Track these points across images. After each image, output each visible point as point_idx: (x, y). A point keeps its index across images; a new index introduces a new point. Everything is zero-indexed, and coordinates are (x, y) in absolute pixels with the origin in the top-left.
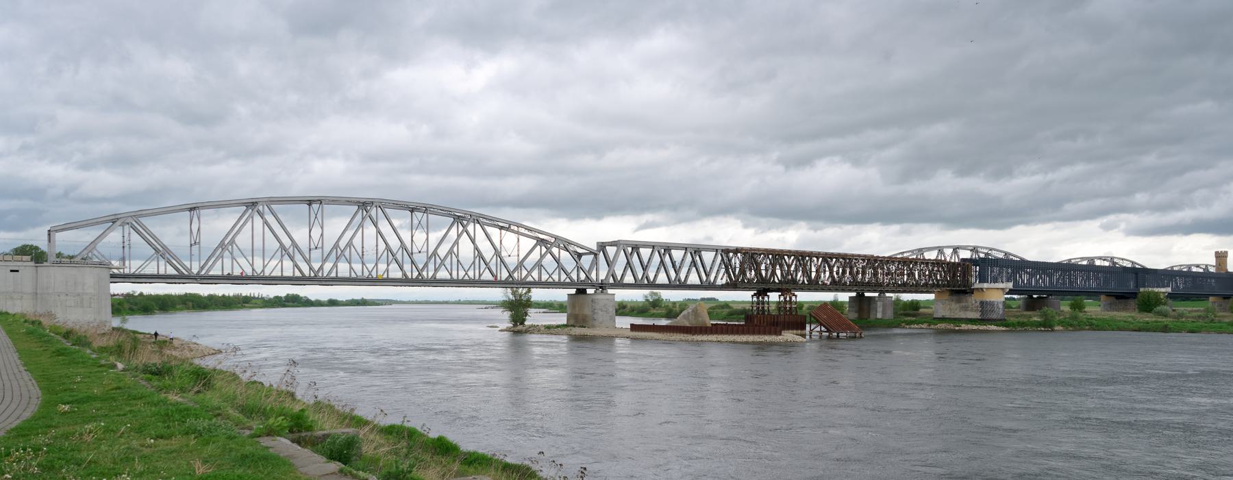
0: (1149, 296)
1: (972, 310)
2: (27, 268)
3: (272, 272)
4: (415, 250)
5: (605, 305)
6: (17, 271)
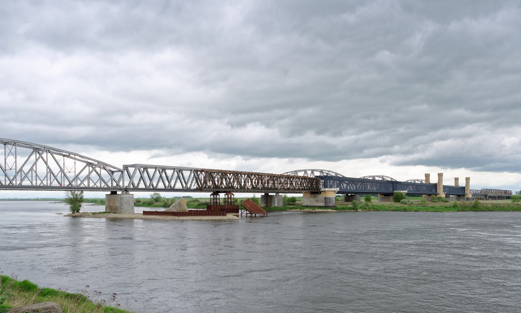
1: (321, 202)
4: (7, 168)
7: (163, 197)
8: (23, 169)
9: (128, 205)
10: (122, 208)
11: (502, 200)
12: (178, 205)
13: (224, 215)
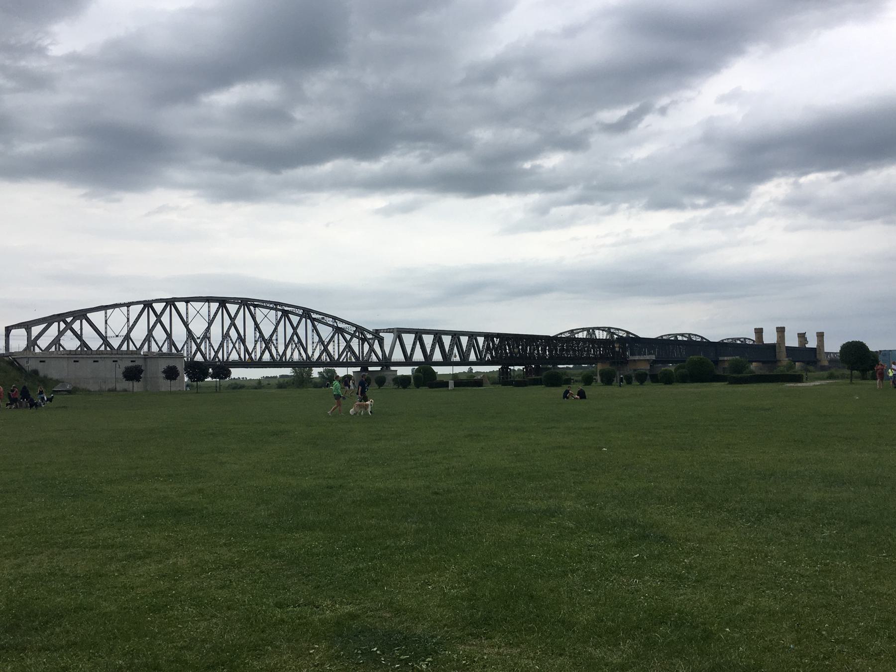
2: (140, 359)
4: (110, 334)
6: (44, 361)
7: (243, 378)
8: (133, 335)
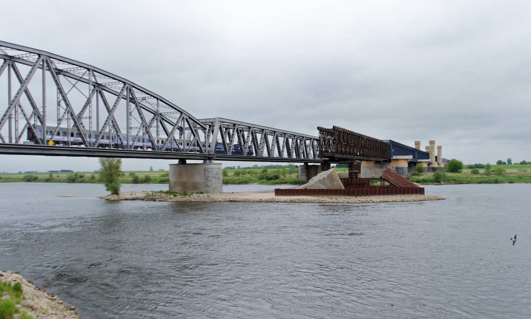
0: (456, 164)
3: (62, 107)
5: (217, 174)
9: (217, 180)
10: (209, 185)
11: (277, 165)
12: (328, 179)
13: (422, 193)
